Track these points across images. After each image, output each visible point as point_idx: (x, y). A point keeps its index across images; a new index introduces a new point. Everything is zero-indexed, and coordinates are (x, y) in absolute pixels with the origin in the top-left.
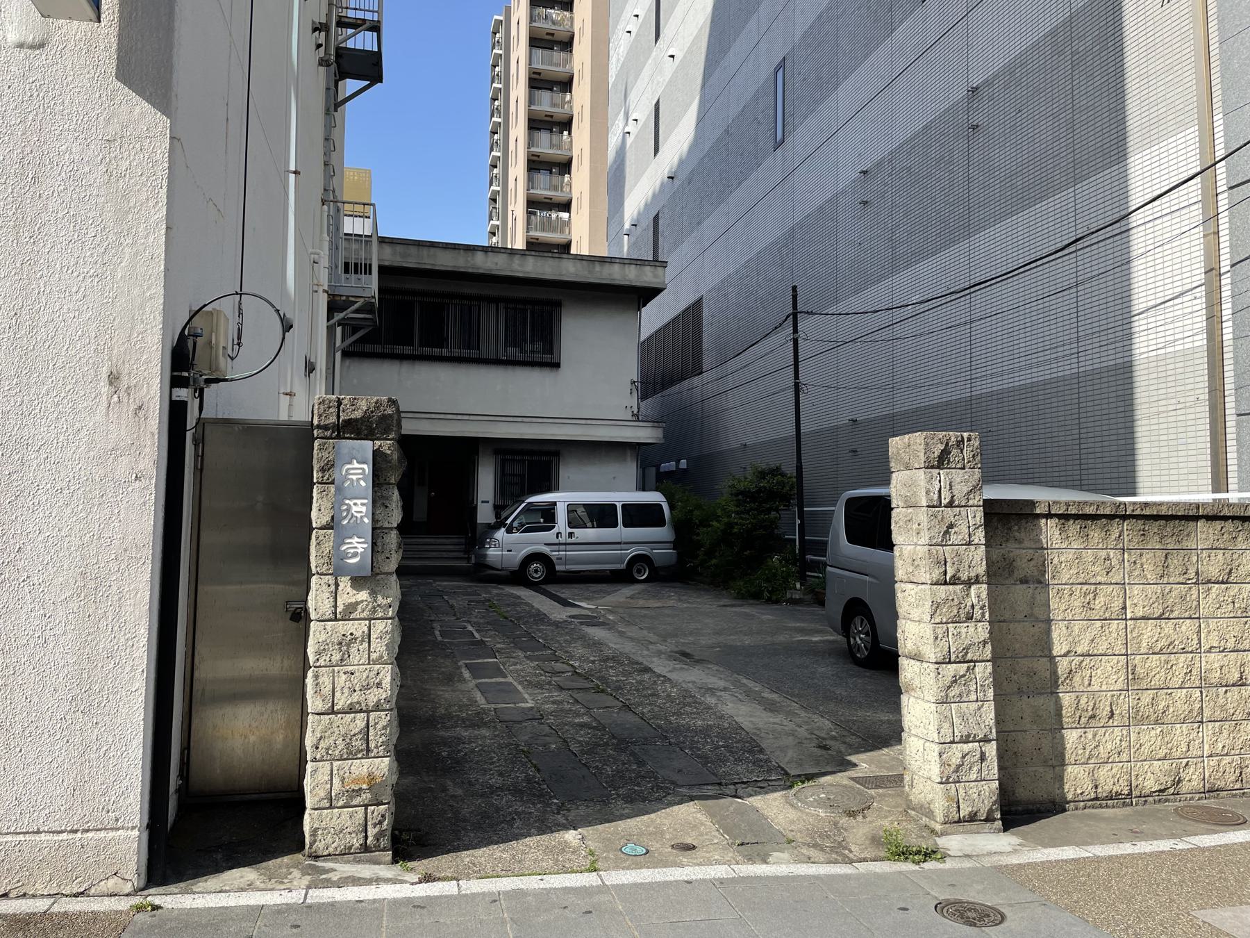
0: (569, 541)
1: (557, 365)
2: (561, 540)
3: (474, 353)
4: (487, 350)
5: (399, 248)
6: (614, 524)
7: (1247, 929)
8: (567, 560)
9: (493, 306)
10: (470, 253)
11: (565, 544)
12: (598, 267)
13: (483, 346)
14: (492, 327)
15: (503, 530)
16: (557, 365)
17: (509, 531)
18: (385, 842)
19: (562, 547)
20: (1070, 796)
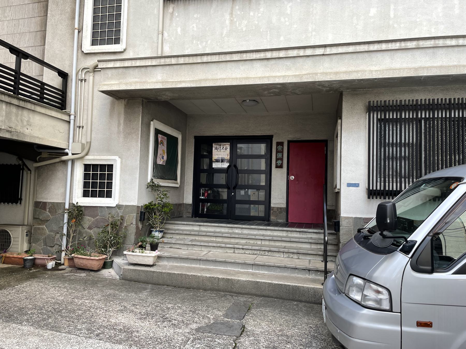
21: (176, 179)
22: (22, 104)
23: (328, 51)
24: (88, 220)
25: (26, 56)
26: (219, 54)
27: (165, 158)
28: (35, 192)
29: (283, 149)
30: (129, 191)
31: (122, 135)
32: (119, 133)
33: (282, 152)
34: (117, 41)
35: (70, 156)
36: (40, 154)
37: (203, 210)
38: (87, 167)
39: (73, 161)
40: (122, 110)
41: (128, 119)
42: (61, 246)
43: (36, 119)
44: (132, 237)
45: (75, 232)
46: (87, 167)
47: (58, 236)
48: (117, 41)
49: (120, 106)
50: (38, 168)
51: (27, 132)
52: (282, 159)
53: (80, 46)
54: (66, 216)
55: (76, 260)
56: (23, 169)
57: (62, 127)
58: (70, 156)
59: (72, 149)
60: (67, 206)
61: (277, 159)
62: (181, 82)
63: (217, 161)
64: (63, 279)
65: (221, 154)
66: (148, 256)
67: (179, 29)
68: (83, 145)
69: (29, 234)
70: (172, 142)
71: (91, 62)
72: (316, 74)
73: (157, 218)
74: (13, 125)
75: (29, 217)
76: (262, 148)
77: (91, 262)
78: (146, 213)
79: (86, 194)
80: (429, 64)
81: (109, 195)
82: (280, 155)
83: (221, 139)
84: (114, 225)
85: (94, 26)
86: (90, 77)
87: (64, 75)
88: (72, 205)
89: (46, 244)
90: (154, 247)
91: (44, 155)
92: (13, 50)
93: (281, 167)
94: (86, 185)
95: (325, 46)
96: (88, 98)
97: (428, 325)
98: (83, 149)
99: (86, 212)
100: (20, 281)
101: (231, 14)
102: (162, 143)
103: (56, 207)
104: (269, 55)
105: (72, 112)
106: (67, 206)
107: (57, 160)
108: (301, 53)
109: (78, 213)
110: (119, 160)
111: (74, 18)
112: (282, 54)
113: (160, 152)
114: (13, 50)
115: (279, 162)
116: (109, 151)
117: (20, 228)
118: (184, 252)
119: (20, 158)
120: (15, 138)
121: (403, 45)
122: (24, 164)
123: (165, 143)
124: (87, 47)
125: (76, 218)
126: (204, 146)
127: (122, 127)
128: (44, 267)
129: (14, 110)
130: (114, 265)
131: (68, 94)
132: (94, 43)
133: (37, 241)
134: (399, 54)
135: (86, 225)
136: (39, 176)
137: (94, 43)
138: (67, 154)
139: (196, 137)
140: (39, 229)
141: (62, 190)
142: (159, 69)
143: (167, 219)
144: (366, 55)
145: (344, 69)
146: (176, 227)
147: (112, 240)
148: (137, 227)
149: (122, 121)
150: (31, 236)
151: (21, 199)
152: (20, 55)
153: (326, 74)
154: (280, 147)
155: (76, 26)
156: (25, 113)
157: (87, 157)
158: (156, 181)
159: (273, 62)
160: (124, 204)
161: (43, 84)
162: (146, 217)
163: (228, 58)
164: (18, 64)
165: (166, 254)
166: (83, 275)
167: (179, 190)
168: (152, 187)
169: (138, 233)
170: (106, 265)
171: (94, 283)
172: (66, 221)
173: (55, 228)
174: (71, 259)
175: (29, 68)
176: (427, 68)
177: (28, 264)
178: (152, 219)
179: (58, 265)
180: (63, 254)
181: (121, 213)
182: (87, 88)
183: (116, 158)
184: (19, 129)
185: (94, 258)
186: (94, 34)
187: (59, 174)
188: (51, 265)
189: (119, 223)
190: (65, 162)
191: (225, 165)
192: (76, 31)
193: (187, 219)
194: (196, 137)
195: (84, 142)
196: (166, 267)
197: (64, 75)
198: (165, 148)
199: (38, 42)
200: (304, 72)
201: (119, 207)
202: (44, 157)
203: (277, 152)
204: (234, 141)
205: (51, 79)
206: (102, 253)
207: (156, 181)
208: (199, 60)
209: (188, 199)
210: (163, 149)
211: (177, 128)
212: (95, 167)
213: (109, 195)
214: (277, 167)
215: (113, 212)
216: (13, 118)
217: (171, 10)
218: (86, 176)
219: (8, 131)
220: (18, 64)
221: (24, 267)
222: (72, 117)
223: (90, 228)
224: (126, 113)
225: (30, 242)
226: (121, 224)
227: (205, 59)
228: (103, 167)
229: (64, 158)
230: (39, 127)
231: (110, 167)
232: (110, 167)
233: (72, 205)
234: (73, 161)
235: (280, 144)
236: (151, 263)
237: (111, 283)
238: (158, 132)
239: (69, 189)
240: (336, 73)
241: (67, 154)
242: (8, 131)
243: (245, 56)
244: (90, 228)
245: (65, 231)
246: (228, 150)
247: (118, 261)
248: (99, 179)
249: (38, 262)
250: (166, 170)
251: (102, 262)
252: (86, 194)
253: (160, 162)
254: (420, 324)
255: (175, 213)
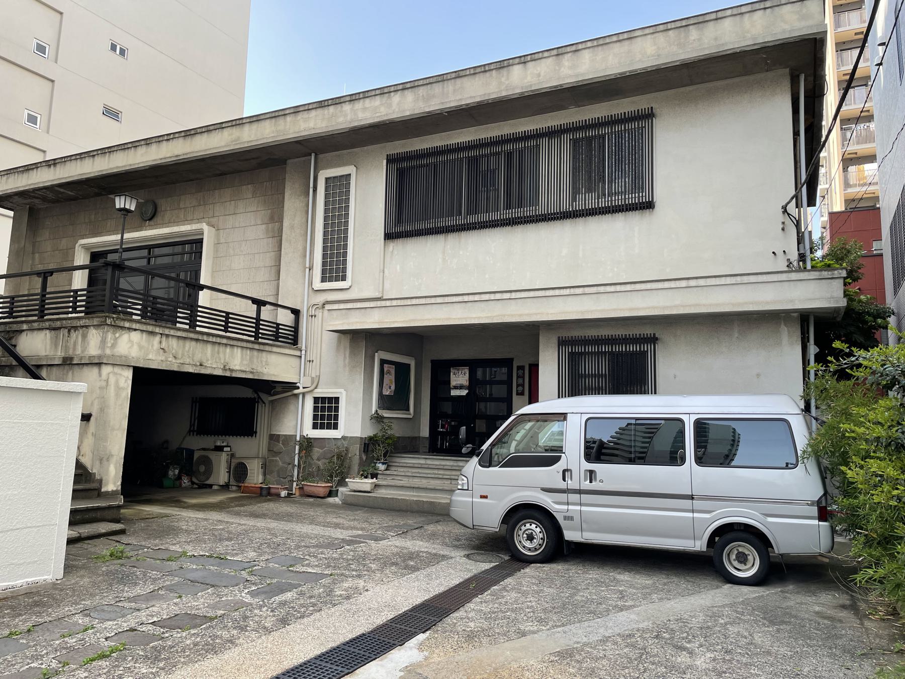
0: (586, 485)
1: (649, 205)
2: (572, 484)
3: (528, 211)
4: (545, 203)
5: (422, 91)
6: (701, 426)
7: (713, 221)
8: (584, 522)
9: (555, 141)
10: (504, 72)
11: (580, 492)
12: (694, 33)
13: (543, 199)
14: (554, 169)
15: (475, 460)
16: (649, 205)
17: (487, 462)
18: (856, 191)
19: (574, 497)
20: (843, 303)
21: (408, 409)
22: (262, 347)
23: (514, 295)
24: (317, 452)
25: (264, 303)
26: (426, 297)
27: (393, 387)
28: (270, 426)
29: (524, 374)
30: (353, 423)
31: (347, 368)
32: (345, 366)
33: (523, 377)
34: (344, 279)
35: (301, 390)
36: (275, 387)
37: (442, 444)
38: (316, 400)
39: (304, 394)
40: (348, 345)
41: (353, 353)
42: (292, 476)
43: (273, 358)
44: (355, 468)
45: (305, 462)
46: (316, 400)
47: (290, 466)
48: (344, 279)
49: (346, 341)
50: (272, 402)
51: (265, 371)
52: (523, 386)
53: (311, 283)
54: (297, 447)
55: (305, 488)
56: (258, 402)
57: (294, 362)
58: (301, 390)
59: (303, 383)
60: (298, 439)
61: (518, 386)
62: (394, 322)
63: (456, 388)
64: (295, 502)
65: (460, 379)
66: (366, 484)
67: (398, 267)
68: (313, 379)
69: (264, 466)
70: (402, 371)
71: (320, 299)
72: (504, 316)
73: (380, 450)
74: (254, 367)
75: (263, 450)
76: (501, 373)
77: (318, 489)
78: (369, 445)
79: (315, 426)
80: (594, 308)
81: (336, 427)
82: (520, 381)
83: (459, 363)
84: (339, 456)
85: (324, 264)
86: (319, 313)
87: (296, 312)
88: (302, 437)
89: (279, 476)
90: (374, 476)
91: (279, 389)
92: (255, 301)
93: (522, 394)
94: (315, 417)
95: (511, 292)
96: (318, 334)
97: (486, 497)
98: (312, 384)
99: (315, 444)
100: (260, 502)
101: (444, 253)
102: (389, 372)
103: (289, 439)
104: (466, 298)
105: (304, 348)
106: (298, 439)
107: (290, 393)
108: (492, 297)
109: (308, 444)
110: (344, 393)
111: (305, 256)
112: (477, 298)
113: (386, 381)
114: (255, 301)
115: (520, 388)
116: (336, 384)
117: (256, 461)
118: (405, 482)
119: (256, 392)
120: (256, 378)
121: (572, 291)
122: (259, 397)
123: (393, 372)
124: (318, 284)
125: (306, 449)
126: (440, 372)
127: (347, 361)
128: (278, 495)
129: (255, 353)
130: (339, 494)
131: (300, 329)
132: (323, 280)
133: (271, 472)
134: (570, 298)
135: (315, 456)
136: (273, 409)
137: (323, 280)
138: (298, 388)
139: (432, 361)
140: (273, 461)
141: (294, 423)
142: (376, 311)
143: (392, 452)
144: (544, 299)
145: (527, 312)
146: (398, 460)
147: (338, 471)
148: (361, 458)
149: (347, 355)
150: (266, 468)
151: (256, 432)
152: (259, 303)
153: (512, 315)
154: (521, 372)
155: (307, 265)
156: (264, 354)
157: (316, 390)
158: (380, 412)
159: (470, 304)
160: (349, 435)
161: (278, 325)
162: (370, 449)
163: (433, 300)
164: (259, 312)
165: (384, 483)
166: (311, 500)
167: (414, 421)
168: (378, 419)
169: (362, 463)
170: (331, 493)
171: (319, 505)
172: (297, 452)
173: (288, 460)
174: (301, 489)
175: (266, 313)
176: (592, 311)
177: (264, 492)
178: (379, 450)
179: (289, 495)
180: (295, 484)
181: (345, 443)
182: (317, 322)
183: (342, 390)
184: (259, 369)
185: (321, 487)
186: (324, 272)
187: (292, 407)
188: (283, 493)
189: (343, 454)
190: (297, 396)
191: (464, 392)
192: (307, 270)
193: (424, 453)
194: (432, 361)
195: (313, 375)
196: (383, 493)
197: (296, 312)
198: (393, 377)
199: (273, 277)
200: (495, 314)
201: (344, 438)
202: (279, 392)
203: (518, 377)
204: (472, 365)
205: (285, 318)
206: (328, 482)
207: (380, 412)
208: (409, 302)
209: (425, 432)
210: (390, 379)
211: (408, 354)
212: (323, 399)
213: (336, 427)
214: (518, 394)
215: (339, 443)
216: (255, 360)
217: (391, 248)
218: (316, 409)
219: (252, 372)
220: (259, 312)
221: (261, 495)
222: (303, 352)
223: (318, 459)
224: (351, 346)
225: (265, 474)
226: (346, 454)
227: (414, 302)
228: (330, 399)
229: (296, 391)
230: (276, 366)
231: (337, 400)
232: (337, 400)
233: (302, 437)
234: (304, 394)
235: (521, 368)
236: (369, 489)
237: (334, 506)
238: (383, 362)
239: (299, 421)
240: (520, 315)
241: (298, 388)
242: (252, 372)
243: (447, 299)
244: (318, 459)
245: (296, 462)
246: (467, 375)
247: (341, 489)
248: (327, 411)
249: (272, 491)
250: (395, 400)
251: (328, 490)
252: (315, 426)
253: (386, 392)
254: (482, 497)
255: (409, 446)
